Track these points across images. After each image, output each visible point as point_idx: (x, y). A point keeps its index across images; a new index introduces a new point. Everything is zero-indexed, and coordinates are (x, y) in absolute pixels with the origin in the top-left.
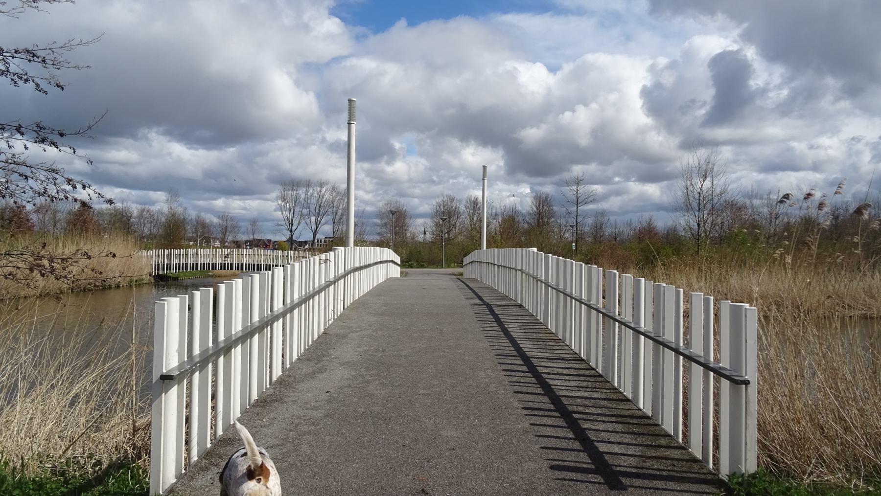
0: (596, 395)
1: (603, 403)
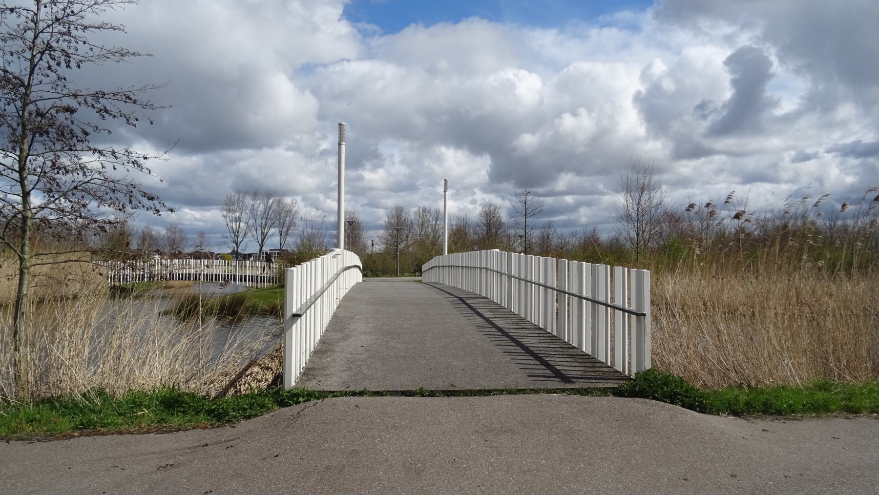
0: (552, 346)
1: (558, 349)
